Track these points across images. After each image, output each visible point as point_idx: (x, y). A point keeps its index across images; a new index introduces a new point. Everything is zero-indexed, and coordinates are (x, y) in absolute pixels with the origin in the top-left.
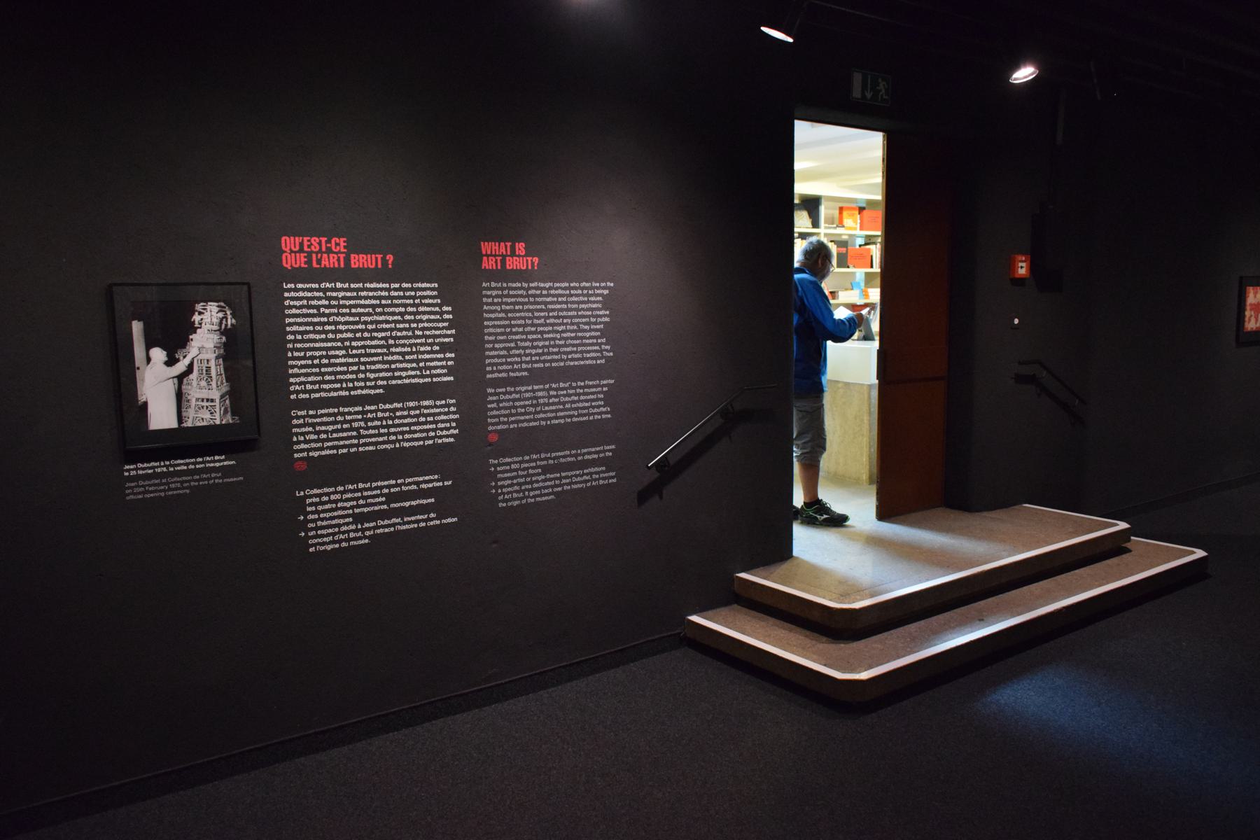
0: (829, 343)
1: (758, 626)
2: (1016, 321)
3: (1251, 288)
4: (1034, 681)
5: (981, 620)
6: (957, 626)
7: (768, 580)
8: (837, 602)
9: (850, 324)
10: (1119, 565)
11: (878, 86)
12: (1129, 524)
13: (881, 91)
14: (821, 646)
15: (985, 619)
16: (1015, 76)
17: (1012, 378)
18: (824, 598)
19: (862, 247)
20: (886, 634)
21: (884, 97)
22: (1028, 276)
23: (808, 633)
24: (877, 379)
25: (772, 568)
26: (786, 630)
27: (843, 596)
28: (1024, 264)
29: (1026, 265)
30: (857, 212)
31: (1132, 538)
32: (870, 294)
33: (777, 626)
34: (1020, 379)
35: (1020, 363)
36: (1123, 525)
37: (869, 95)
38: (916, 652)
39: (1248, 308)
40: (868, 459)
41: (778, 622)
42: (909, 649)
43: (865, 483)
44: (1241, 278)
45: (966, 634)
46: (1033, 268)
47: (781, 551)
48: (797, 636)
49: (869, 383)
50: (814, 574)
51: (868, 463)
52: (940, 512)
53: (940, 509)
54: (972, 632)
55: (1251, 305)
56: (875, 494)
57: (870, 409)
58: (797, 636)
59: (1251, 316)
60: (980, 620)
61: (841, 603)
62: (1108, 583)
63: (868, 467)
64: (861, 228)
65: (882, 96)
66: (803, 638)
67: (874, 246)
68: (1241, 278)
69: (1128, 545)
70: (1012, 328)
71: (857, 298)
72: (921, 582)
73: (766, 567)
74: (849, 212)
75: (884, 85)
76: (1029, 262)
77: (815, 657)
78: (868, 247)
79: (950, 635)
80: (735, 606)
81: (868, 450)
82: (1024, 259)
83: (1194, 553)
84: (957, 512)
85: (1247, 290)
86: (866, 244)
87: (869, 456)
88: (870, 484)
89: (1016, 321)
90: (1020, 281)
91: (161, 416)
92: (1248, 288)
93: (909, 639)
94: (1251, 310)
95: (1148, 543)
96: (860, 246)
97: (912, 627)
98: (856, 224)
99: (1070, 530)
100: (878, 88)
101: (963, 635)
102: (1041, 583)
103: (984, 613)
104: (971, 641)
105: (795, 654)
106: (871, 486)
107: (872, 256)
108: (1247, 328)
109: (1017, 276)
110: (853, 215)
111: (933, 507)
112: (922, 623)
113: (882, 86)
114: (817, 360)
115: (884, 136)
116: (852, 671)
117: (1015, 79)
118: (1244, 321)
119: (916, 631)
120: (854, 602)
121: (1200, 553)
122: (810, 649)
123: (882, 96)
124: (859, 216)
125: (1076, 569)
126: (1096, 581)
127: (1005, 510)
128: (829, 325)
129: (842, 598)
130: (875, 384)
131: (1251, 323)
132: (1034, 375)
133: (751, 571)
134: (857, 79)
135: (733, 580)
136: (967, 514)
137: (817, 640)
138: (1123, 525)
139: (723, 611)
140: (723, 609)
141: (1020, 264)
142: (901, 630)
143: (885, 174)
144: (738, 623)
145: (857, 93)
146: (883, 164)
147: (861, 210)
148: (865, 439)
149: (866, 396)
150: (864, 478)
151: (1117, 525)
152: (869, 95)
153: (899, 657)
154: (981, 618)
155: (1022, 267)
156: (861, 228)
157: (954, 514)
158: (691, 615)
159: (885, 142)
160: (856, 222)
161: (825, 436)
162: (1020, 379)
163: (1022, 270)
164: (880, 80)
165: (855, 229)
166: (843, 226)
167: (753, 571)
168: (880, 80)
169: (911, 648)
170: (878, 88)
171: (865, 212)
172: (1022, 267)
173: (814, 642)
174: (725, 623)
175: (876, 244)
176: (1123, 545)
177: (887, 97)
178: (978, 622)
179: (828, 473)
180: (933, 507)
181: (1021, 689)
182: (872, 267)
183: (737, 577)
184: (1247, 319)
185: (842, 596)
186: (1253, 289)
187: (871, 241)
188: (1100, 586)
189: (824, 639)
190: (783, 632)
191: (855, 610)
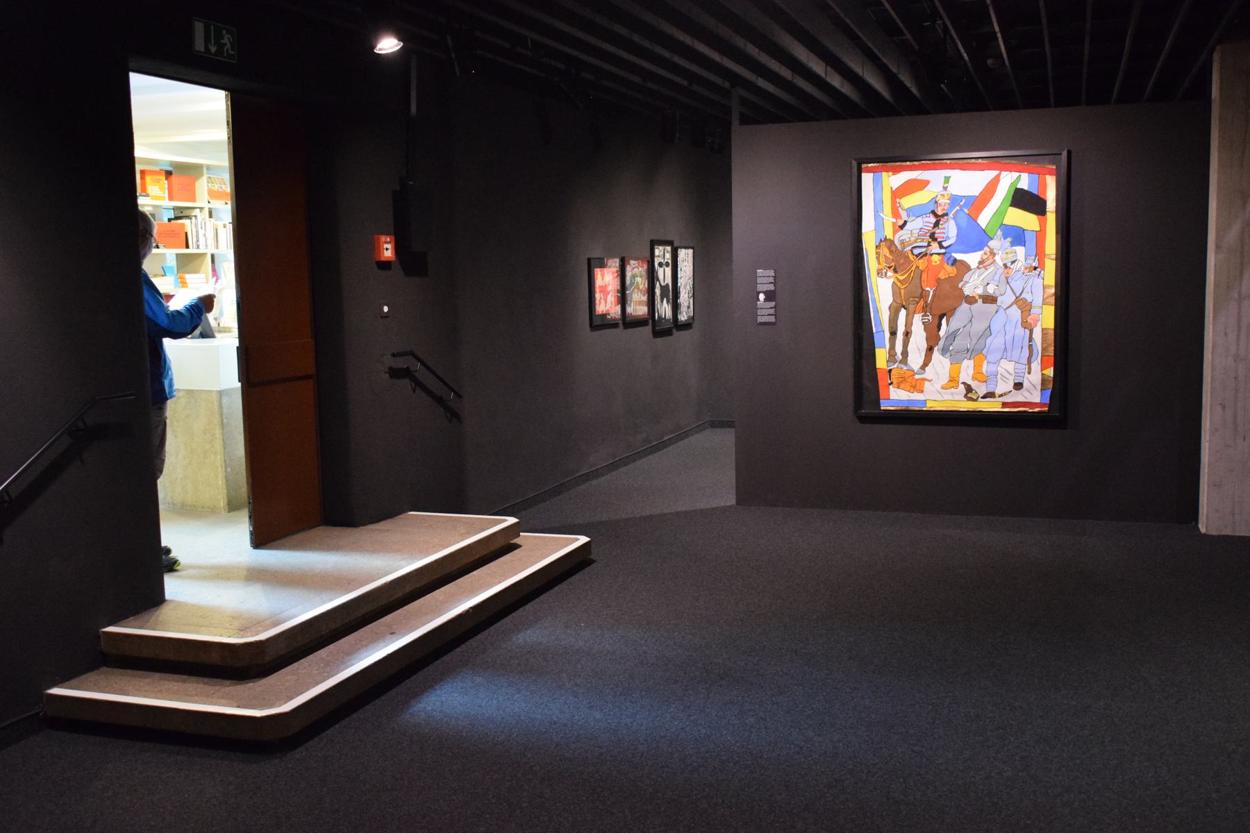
0: (167, 342)
1: (142, 684)
2: (386, 309)
3: (599, 269)
4: (455, 684)
5: (393, 633)
6: (369, 643)
7: (146, 629)
8: (237, 637)
9: (192, 315)
10: (512, 561)
11: (223, 39)
12: (518, 518)
13: (226, 44)
14: (227, 689)
15: (396, 632)
16: (379, 46)
17: (386, 373)
18: (221, 636)
19: (173, 222)
20: (296, 665)
21: (230, 52)
22: (394, 259)
23: (206, 680)
24: (239, 381)
25: (145, 616)
26: (179, 682)
27: (243, 630)
28: (389, 246)
29: (392, 246)
30: (163, 178)
31: (521, 534)
32: (188, 281)
33: (166, 680)
34: (395, 373)
35: (393, 355)
36: (512, 520)
37: (213, 49)
38: (334, 675)
39: (597, 290)
40: (224, 480)
41: (163, 675)
42: (326, 674)
43: (223, 512)
44: (589, 260)
45: (381, 649)
46: (398, 250)
47: (155, 598)
48: (193, 685)
49: (219, 390)
50: (203, 615)
51: (225, 487)
52: (321, 531)
53: (321, 527)
54: (387, 646)
55: (600, 287)
56: (247, 519)
57: (222, 421)
58: (195, 685)
59: (601, 298)
60: (392, 633)
61: (243, 637)
62: (506, 579)
63: (225, 491)
64: (171, 199)
65: (227, 50)
66: (202, 686)
67: (189, 220)
68: (589, 260)
69: (516, 541)
70: (382, 317)
71: (173, 287)
72: (324, 603)
73: (137, 616)
74: (154, 177)
75: (229, 38)
76: (393, 242)
77: (223, 701)
78: (180, 221)
79: (365, 654)
80: (104, 669)
81: (224, 469)
82: (388, 240)
83: (577, 540)
84: (338, 529)
85: (595, 273)
86: (177, 218)
87: (226, 478)
88: (229, 512)
89: (386, 309)
90: (385, 265)
91: (607, 305)
92: (596, 269)
93: (322, 665)
94: (600, 292)
95: (535, 537)
96: (170, 220)
97: (323, 653)
98: (164, 193)
99: (463, 531)
100: (222, 41)
101: (379, 650)
102: (442, 589)
103: (394, 627)
104: (388, 655)
105: (200, 703)
106: (231, 513)
107: (186, 233)
108: (599, 311)
109: (383, 259)
110: (158, 181)
111: (311, 527)
112: (332, 647)
113: (227, 39)
114: (158, 362)
115: (226, 96)
116: (271, 706)
117: (380, 50)
118: (595, 304)
119: (327, 656)
120: (258, 634)
121: (583, 539)
122: (214, 695)
123: (227, 50)
124: (166, 182)
125: (473, 571)
126: (496, 579)
127: (390, 520)
128: (164, 322)
129: (242, 632)
130: (237, 388)
131: (601, 305)
132: (408, 368)
133: (119, 623)
134: (199, 27)
135: (99, 637)
136: (348, 530)
137: (220, 685)
138: (512, 520)
139: (91, 677)
140: (89, 674)
141: (386, 246)
142: (311, 657)
143: (231, 140)
144: (114, 685)
145: (199, 45)
146: (228, 128)
147: (168, 174)
148: (219, 457)
149: (216, 408)
150: (222, 505)
151: (506, 520)
152: (213, 49)
153: (317, 683)
154: (393, 631)
155: (387, 249)
156: (171, 199)
157: (337, 531)
158: (50, 688)
159: (229, 103)
160: (162, 189)
161: (164, 456)
162: (395, 373)
163: (388, 252)
164: (224, 32)
165: (162, 199)
166: (147, 195)
167: (122, 623)
168: (224, 32)
169: (327, 672)
170: (222, 41)
171: (174, 178)
172: (387, 249)
173: (217, 688)
174: (98, 688)
175: (191, 219)
176: (512, 542)
177: (233, 53)
178: (390, 636)
179: (173, 504)
180: (313, 528)
181: (445, 693)
182: (187, 247)
183: (104, 632)
184: (597, 302)
185: (242, 631)
186: (601, 271)
187: (184, 214)
188: (500, 582)
189: (228, 682)
190: (176, 684)
191: (261, 642)
